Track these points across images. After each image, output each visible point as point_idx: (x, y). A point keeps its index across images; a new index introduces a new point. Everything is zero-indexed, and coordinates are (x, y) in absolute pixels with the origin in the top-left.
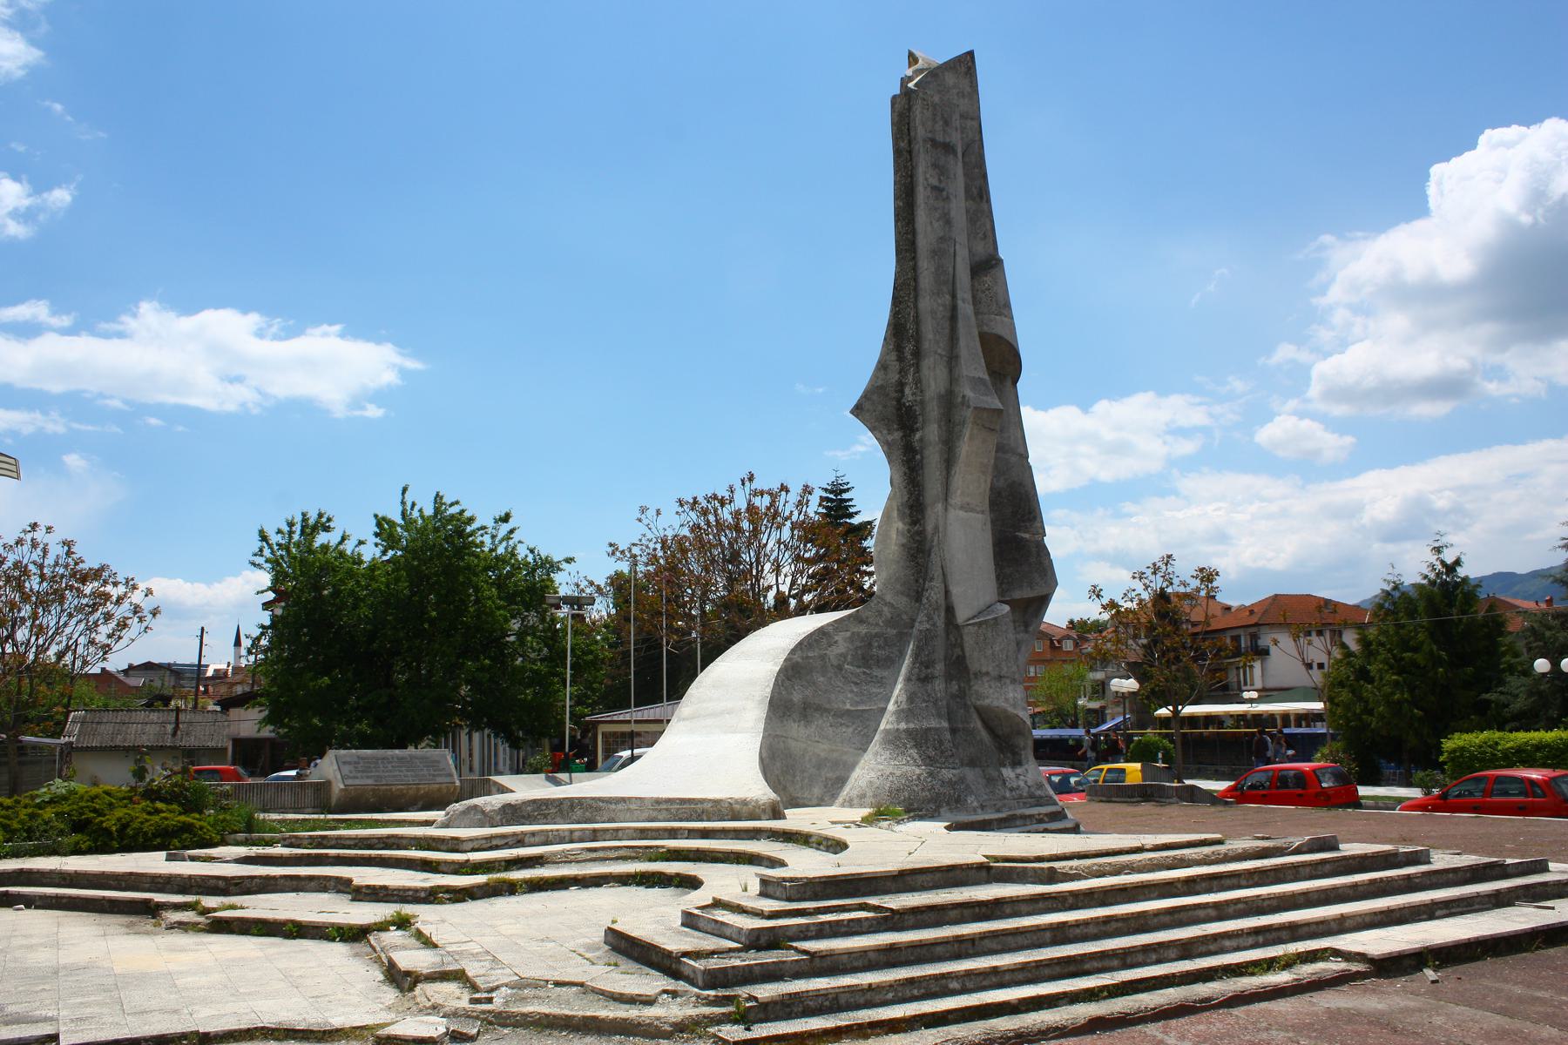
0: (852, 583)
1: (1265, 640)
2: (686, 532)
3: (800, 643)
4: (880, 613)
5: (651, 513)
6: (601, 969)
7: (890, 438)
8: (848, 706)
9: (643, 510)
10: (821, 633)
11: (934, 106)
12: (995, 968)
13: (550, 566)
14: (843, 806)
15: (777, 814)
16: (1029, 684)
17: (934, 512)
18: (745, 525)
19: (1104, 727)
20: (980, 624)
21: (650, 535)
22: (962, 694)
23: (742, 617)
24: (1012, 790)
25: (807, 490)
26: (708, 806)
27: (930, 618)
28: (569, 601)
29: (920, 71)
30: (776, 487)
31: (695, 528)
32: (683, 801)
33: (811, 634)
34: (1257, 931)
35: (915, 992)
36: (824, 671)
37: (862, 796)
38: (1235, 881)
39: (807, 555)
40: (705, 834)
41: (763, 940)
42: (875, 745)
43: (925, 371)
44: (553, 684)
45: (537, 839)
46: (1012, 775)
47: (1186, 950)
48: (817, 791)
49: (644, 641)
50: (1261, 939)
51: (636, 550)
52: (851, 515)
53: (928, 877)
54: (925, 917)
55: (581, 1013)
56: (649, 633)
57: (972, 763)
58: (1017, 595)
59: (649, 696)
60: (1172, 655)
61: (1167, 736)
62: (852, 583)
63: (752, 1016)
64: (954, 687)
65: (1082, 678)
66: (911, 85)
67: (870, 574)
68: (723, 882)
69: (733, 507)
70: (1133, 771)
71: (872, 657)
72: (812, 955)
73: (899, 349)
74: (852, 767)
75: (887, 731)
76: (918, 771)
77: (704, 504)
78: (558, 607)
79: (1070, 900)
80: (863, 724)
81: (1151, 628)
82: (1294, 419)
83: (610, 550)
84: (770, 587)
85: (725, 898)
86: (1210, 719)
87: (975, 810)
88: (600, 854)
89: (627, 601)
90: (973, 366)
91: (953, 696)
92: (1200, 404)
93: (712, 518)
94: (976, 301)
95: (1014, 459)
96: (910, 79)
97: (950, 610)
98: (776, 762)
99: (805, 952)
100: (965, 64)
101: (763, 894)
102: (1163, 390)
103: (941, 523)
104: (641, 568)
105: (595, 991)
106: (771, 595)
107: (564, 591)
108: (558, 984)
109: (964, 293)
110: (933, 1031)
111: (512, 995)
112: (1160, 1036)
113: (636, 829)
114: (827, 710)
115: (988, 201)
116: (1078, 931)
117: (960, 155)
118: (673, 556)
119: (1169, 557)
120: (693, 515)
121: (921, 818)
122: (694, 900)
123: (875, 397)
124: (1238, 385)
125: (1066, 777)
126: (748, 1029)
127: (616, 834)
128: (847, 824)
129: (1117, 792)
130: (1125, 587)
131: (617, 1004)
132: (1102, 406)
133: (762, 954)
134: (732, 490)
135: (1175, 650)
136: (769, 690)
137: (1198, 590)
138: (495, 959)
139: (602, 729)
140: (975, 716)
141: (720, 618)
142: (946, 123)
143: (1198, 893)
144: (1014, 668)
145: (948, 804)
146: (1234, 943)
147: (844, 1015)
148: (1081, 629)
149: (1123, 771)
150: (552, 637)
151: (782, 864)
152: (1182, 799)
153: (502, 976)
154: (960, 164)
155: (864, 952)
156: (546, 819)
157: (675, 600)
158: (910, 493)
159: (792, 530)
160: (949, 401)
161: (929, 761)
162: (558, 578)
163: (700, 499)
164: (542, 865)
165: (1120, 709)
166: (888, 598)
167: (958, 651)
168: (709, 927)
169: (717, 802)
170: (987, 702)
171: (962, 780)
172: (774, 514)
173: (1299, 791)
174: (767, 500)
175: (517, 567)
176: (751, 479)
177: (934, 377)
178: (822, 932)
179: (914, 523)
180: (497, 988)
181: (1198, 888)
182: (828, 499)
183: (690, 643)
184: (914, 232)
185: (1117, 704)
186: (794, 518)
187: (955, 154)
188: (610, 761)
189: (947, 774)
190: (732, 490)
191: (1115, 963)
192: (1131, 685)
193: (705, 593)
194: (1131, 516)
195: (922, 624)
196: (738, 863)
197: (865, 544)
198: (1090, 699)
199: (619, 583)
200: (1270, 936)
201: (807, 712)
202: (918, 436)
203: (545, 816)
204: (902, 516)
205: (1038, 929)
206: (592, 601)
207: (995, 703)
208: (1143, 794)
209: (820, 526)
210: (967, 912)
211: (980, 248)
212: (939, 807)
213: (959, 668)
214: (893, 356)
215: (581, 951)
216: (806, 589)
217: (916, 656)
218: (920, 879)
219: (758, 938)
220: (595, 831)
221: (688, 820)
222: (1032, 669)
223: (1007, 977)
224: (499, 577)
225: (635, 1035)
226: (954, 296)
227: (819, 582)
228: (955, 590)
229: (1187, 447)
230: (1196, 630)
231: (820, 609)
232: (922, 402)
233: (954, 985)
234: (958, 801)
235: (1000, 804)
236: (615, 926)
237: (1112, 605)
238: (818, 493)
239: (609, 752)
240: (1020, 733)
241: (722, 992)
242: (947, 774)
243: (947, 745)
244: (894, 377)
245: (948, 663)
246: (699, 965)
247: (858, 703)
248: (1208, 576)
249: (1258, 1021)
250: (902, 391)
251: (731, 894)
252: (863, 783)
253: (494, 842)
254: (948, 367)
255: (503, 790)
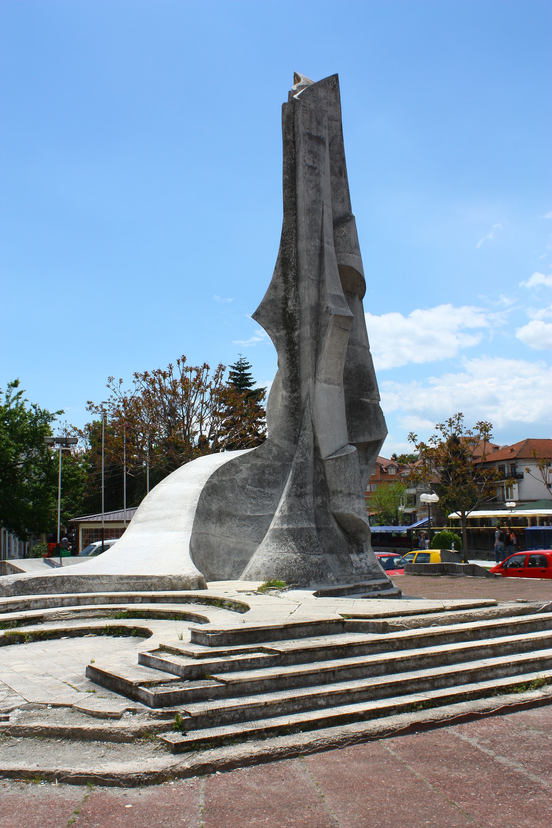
0: (250, 430)
1: (521, 469)
2: (139, 394)
3: (217, 471)
4: (270, 451)
5: (116, 381)
6: (83, 695)
7: (278, 335)
8: (249, 513)
9: (111, 379)
10: (231, 464)
11: (311, 111)
12: (348, 690)
13: (47, 417)
14: (245, 580)
15: (201, 586)
16: (367, 497)
17: (307, 385)
18: (180, 390)
19: (415, 525)
20: (336, 459)
21: (115, 397)
22: (324, 505)
23: (177, 453)
24: (357, 569)
25: (221, 368)
26: (155, 581)
27: (303, 455)
28: (59, 441)
29: (302, 87)
30: (200, 365)
31: (146, 392)
32: (138, 578)
33: (224, 465)
34: (519, 664)
35: (296, 707)
36: (233, 490)
37: (258, 573)
38: (504, 630)
39: (221, 411)
40: (153, 600)
41: (194, 674)
42: (266, 539)
43: (302, 290)
44: (48, 496)
45: (39, 605)
46: (357, 559)
47: (473, 676)
48: (228, 570)
49: (111, 468)
50: (521, 669)
51: (106, 407)
52: (250, 385)
53: (304, 629)
54: (302, 656)
55: (70, 726)
56: (113, 463)
57: (331, 551)
58: (361, 439)
59: (114, 505)
60: (461, 479)
61: (456, 531)
62: (250, 430)
63: (187, 726)
64: (319, 500)
65: (401, 492)
66: (295, 96)
67: (263, 424)
68: (166, 633)
69: (172, 379)
70: (435, 555)
71: (265, 481)
72: (227, 683)
73: (285, 275)
74: (251, 554)
75: (274, 530)
76: (295, 557)
77: (152, 376)
78: (52, 445)
79: (397, 644)
80: (259, 524)
81: (448, 461)
82: (543, 323)
83: (88, 406)
84: (196, 433)
85: (168, 645)
86: (485, 521)
87: (333, 582)
88: (82, 614)
89: (100, 441)
90: (334, 287)
91: (319, 507)
92: (481, 313)
93: (157, 386)
94: (336, 244)
95: (360, 350)
96: (295, 92)
97: (317, 449)
98: (200, 551)
99: (222, 681)
100: (332, 83)
101: (194, 642)
102: (457, 304)
103: (311, 391)
104: (109, 418)
105: (80, 710)
106: (197, 438)
107: (56, 434)
108: (54, 706)
109: (329, 239)
110: (308, 733)
111: (22, 715)
112: (457, 735)
113: (106, 597)
114: (234, 516)
115: (346, 177)
116: (402, 665)
117: (327, 145)
118: (131, 411)
119: (460, 414)
120: (145, 384)
121: (297, 588)
122: (147, 645)
123: (268, 307)
124: (506, 301)
125: (391, 558)
126: (184, 735)
127: (93, 600)
128: (249, 593)
129: (424, 569)
130: (431, 435)
131: (95, 720)
132: (417, 314)
133: (193, 683)
134: (171, 367)
135: (463, 475)
136: (196, 502)
137: (479, 437)
138: (10, 690)
139: (82, 527)
140: (333, 520)
141: (162, 452)
142: (319, 123)
143: (480, 639)
144: (359, 489)
145: (315, 578)
146: (504, 672)
147: (248, 724)
148: (401, 461)
149: (428, 555)
150: (48, 466)
151: (206, 621)
152: (467, 574)
153: (15, 701)
154: (327, 151)
155: (261, 681)
156: (45, 590)
157: (131, 441)
158: (291, 372)
159: (211, 394)
160: (318, 311)
161: (302, 550)
162: (52, 425)
163: (150, 373)
164: (42, 622)
165: (426, 513)
166: (276, 441)
167: (322, 477)
168: (158, 665)
169: (161, 578)
170: (341, 511)
171: (324, 562)
172: (199, 384)
173: (543, 568)
174: (194, 374)
175: (24, 418)
176: (184, 360)
177: (308, 294)
178: (234, 667)
179: (293, 391)
180: (12, 710)
181: (481, 635)
182: (235, 374)
183: (142, 469)
184: (296, 197)
185: (424, 510)
186: (213, 386)
187: (324, 144)
188: (88, 548)
189: (314, 558)
190: (171, 367)
191: (427, 686)
192: (433, 498)
193: (152, 436)
194: (434, 385)
195: (298, 459)
196: (176, 619)
197: (259, 403)
198: (406, 507)
199: (95, 432)
200: (527, 667)
201: (221, 517)
202: (297, 333)
203: (45, 589)
204: (285, 387)
205: (376, 664)
206: (75, 441)
207: (346, 512)
208: (442, 570)
209: (230, 391)
210: (329, 653)
211: (340, 208)
212: (309, 580)
213: (322, 488)
214: (281, 280)
215: (70, 682)
216: (220, 434)
217: (294, 479)
218: (298, 630)
219: (191, 672)
220: (78, 598)
221: (141, 590)
222: (368, 487)
223: (357, 696)
224: (12, 424)
225: (108, 741)
226: (322, 240)
227: (228, 429)
228: (320, 437)
229: (472, 341)
230: (475, 462)
231: (230, 447)
232: (300, 311)
233: (322, 702)
234: (321, 576)
235: (349, 578)
236: (93, 665)
237: (422, 445)
238: (229, 369)
239: (87, 543)
240: (362, 531)
241: (166, 710)
242: (314, 558)
243: (315, 539)
244: (281, 293)
245: (316, 485)
246: (151, 691)
247: (255, 511)
248: (485, 427)
249: (520, 723)
250: (286, 304)
251: (172, 642)
252: (259, 564)
253: (9, 607)
254: (317, 288)
255: (16, 570)
